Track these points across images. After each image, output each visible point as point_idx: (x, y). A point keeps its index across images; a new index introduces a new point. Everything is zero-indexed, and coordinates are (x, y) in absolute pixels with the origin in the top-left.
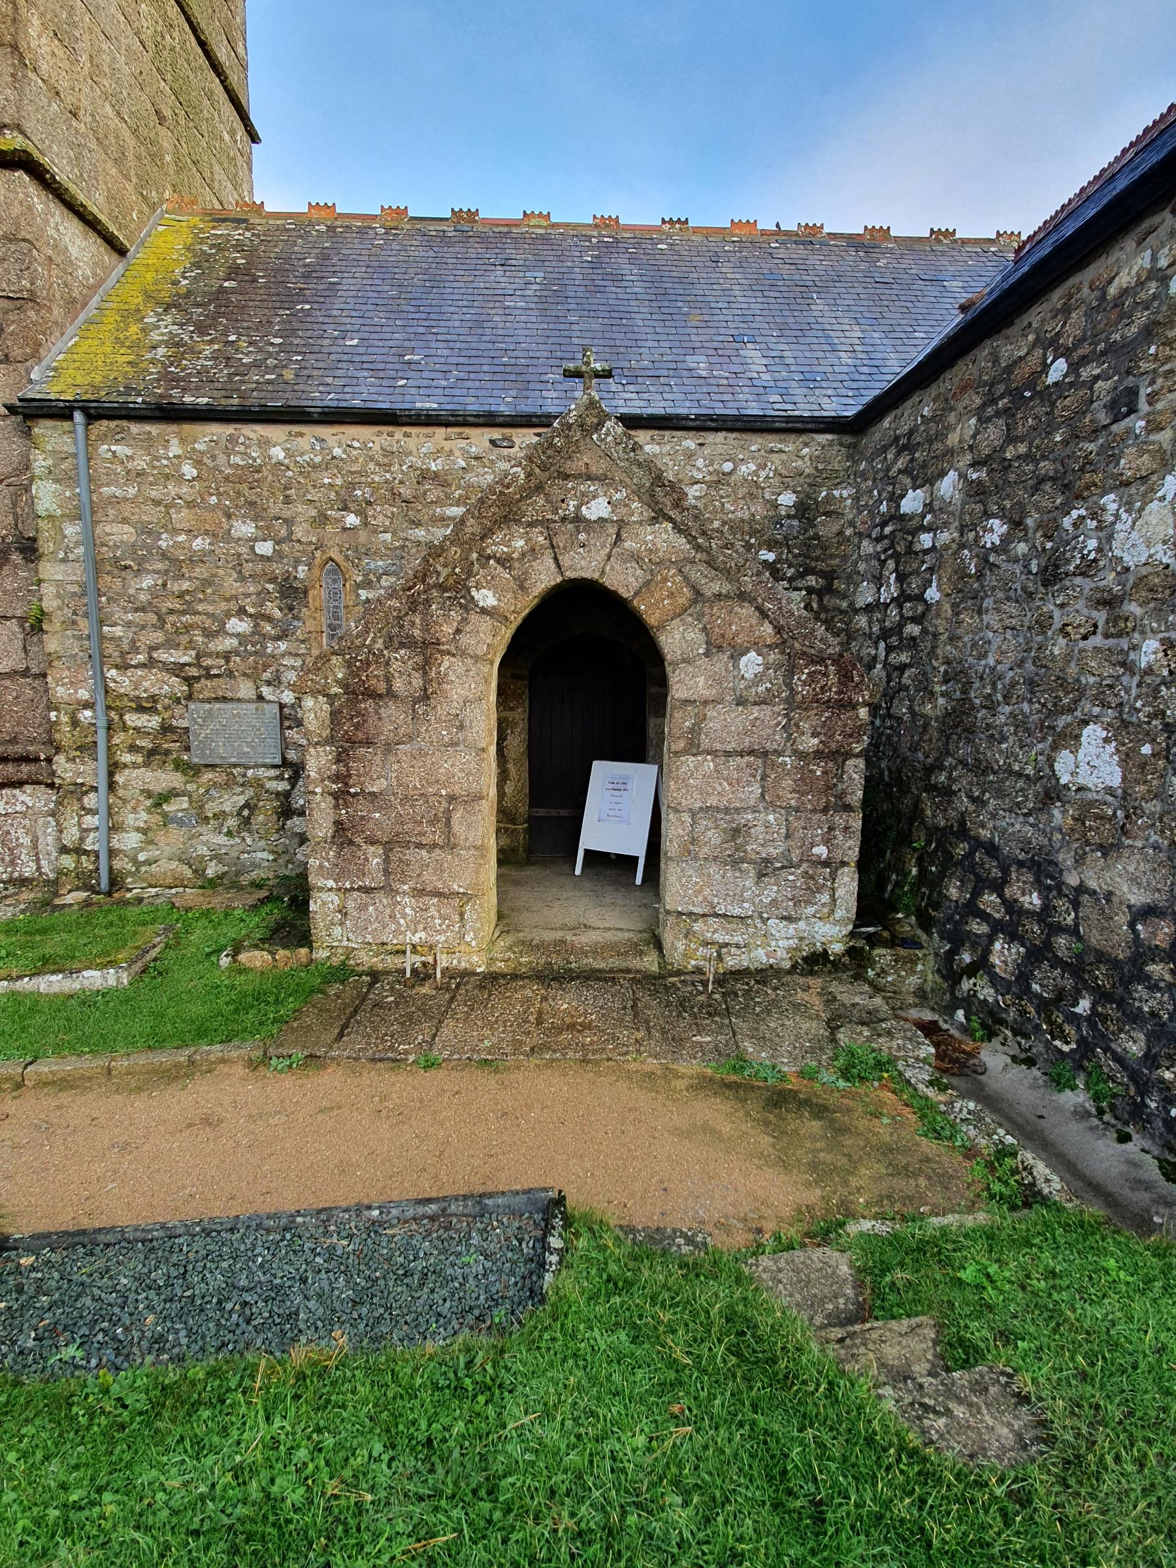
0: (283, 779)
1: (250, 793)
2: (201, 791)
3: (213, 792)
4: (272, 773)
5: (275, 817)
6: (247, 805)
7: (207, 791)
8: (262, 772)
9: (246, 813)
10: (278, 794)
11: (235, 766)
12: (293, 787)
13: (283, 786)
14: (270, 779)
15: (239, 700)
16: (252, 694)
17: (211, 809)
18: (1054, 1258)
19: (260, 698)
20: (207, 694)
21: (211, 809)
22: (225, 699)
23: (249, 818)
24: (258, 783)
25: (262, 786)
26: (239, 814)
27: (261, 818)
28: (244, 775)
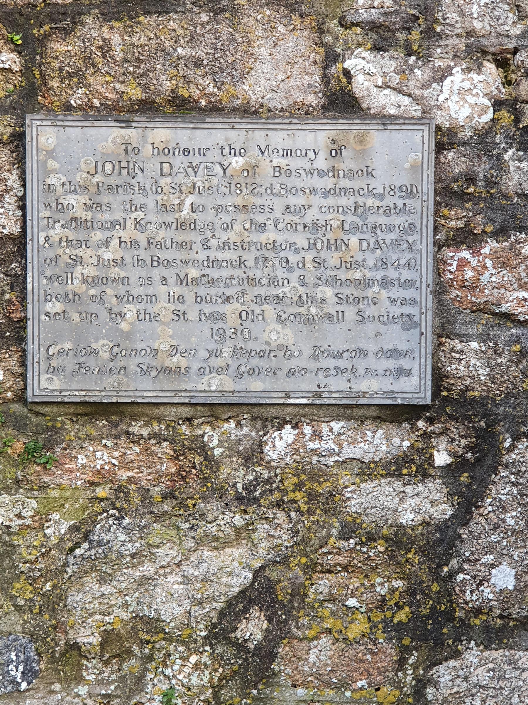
0: (424, 471)
1: (274, 532)
2: (58, 526)
3: (117, 537)
4: (380, 443)
5: (389, 652)
6: (259, 594)
7: (82, 531)
8: (337, 442)
9: (253, 628)
10: (399, 540)
11: (214, 411)
12: (467, 503)
13: (421, 504)
14: (366, 470)
15: (248, 111)
16: (304, 85)
17: (94, 607)
18: (204, 608)
19: (341, 102)
20: (103, 86)
21: (94, 607)
22: (182, 107)
23: (266, 653)
24: (312, 491)
25: (329, 503)
26: (221, 631)
27: (320, 653)
28: (253, 456)
